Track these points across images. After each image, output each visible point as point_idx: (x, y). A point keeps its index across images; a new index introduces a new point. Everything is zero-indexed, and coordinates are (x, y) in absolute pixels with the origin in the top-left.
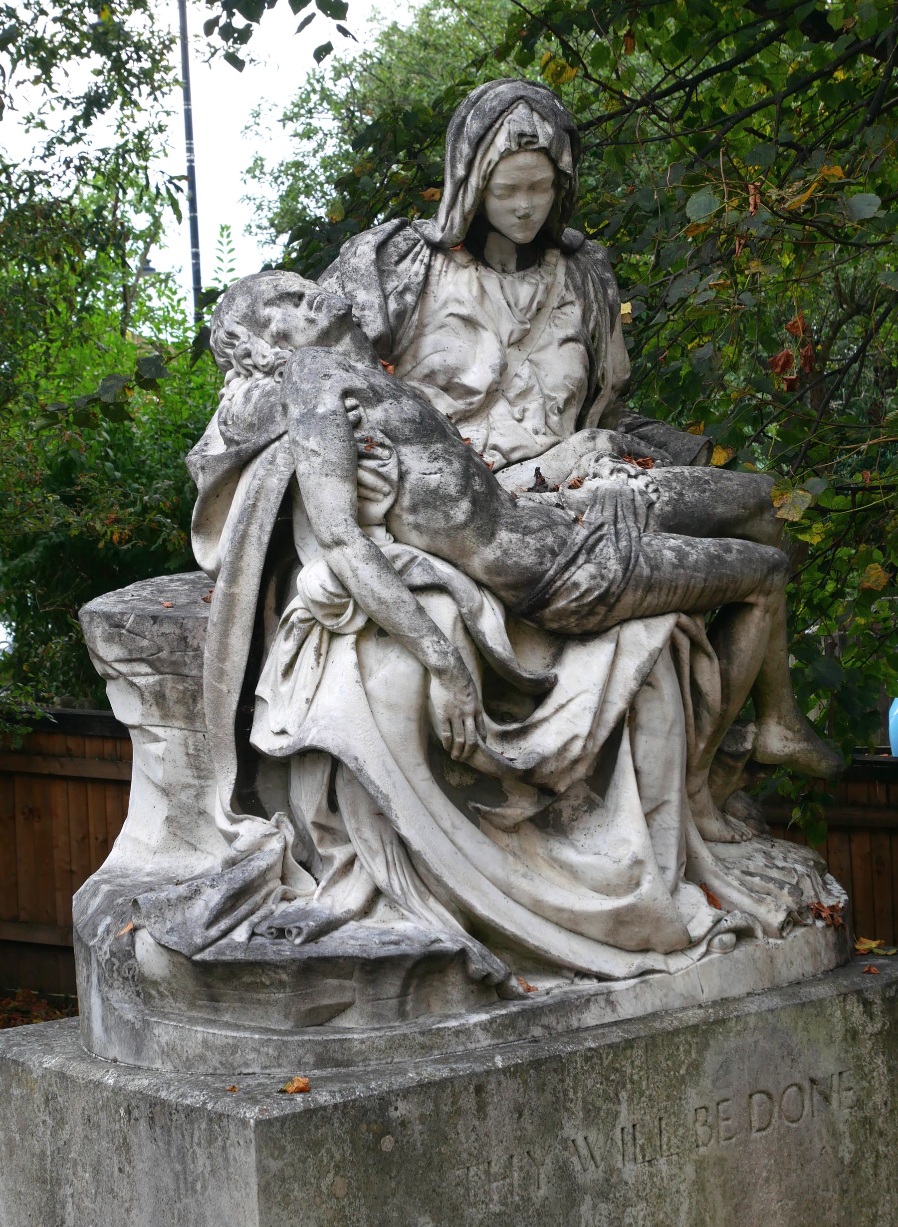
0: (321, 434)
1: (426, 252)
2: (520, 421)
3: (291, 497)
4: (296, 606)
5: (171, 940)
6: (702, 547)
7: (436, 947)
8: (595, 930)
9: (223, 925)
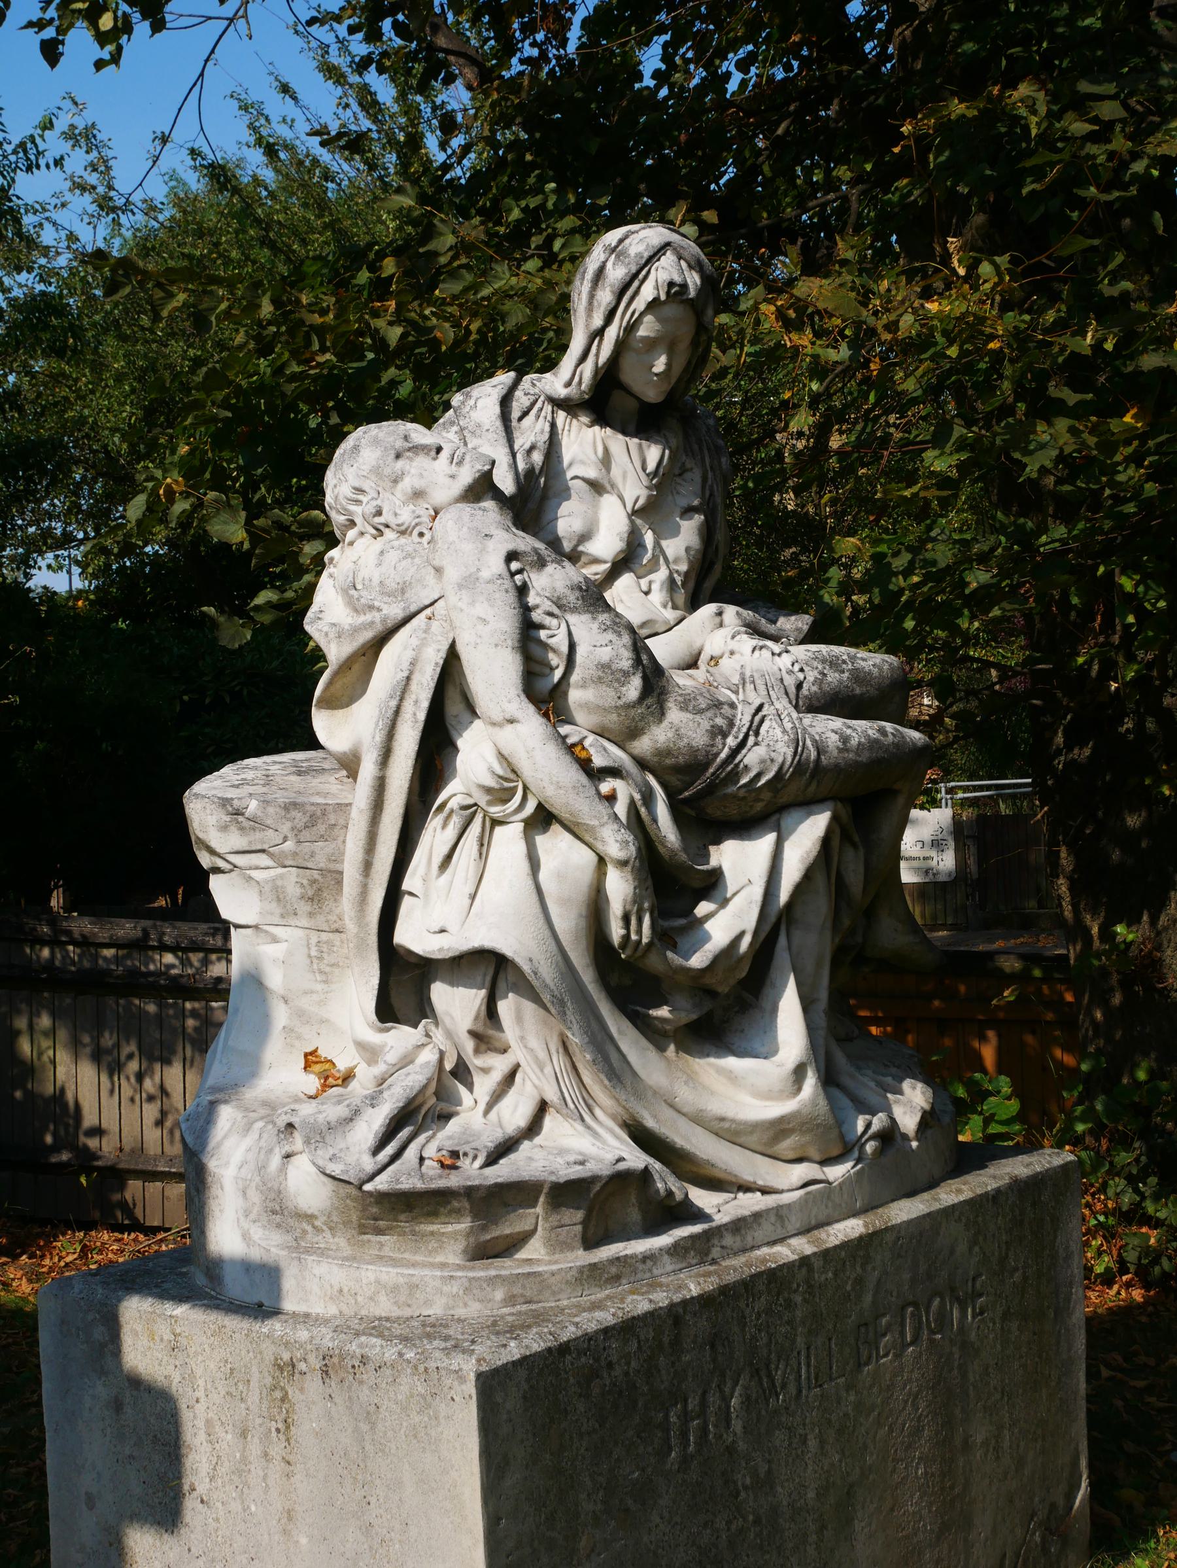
0: (489, 600)
1: (548, 408)
2: (646, 593)
3: (451, 668)
4: (454, 792)
5: (336, 1169)
6: (862, 729)
7: (622, 1166)
8: (752, 1140)
9: (389, 1150)
